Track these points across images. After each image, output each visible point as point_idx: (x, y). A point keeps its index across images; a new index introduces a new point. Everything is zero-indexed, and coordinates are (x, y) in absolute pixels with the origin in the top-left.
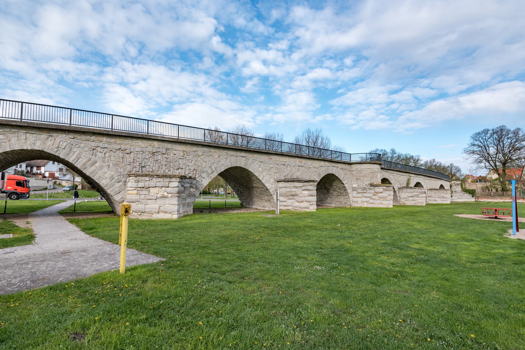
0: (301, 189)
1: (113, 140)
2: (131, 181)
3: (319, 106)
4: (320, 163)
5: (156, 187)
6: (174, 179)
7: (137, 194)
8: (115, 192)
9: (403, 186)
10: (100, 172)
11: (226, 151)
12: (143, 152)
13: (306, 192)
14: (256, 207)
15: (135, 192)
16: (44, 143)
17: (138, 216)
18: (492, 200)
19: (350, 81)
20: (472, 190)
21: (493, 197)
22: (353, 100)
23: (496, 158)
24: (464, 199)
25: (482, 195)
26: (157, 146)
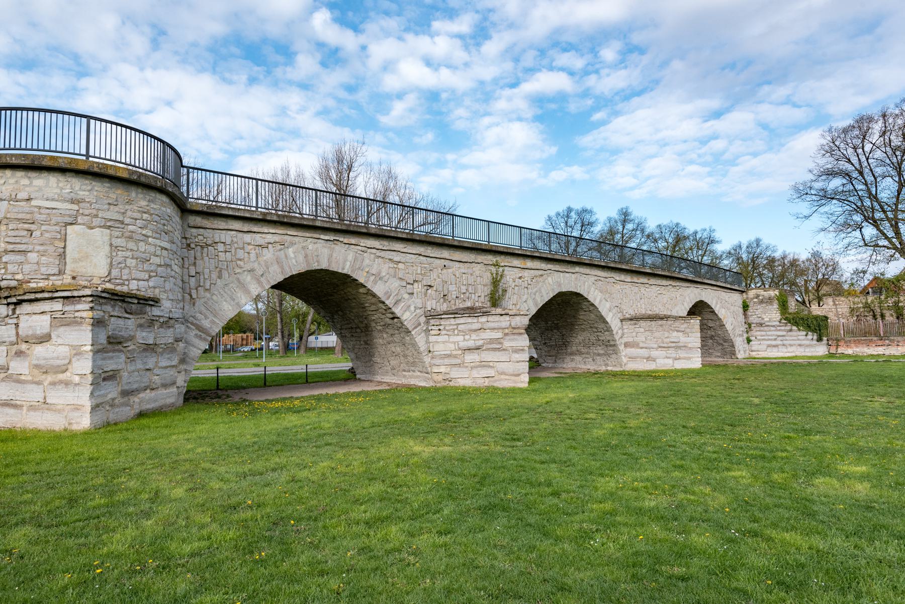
3: (554, 150)
19: (617, 94)
22: (628, 134)
24: (790, 349)
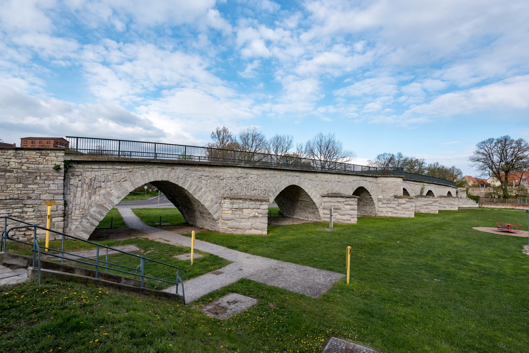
0: (343, 204)
1: (212, 169)
2: (227, 203)
4: (353, 178)
5: (248, 208)
6: (264, 203)
7: (232, 214)
8: (214, 212)
9: (418, 194)
10: (205, 196)
11: (285, 172)
12: (231, 178)
13: (348, 207)
14: (298, 218)
15: (231, 211)
16: (169, 175)
17: (233, 232)
18: (494, 207)
20: (476, 196)
21: (496, 203)
23: (499, 166)
24: (469, 205)
25: (485, 201)
26: (240, 172)
